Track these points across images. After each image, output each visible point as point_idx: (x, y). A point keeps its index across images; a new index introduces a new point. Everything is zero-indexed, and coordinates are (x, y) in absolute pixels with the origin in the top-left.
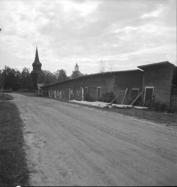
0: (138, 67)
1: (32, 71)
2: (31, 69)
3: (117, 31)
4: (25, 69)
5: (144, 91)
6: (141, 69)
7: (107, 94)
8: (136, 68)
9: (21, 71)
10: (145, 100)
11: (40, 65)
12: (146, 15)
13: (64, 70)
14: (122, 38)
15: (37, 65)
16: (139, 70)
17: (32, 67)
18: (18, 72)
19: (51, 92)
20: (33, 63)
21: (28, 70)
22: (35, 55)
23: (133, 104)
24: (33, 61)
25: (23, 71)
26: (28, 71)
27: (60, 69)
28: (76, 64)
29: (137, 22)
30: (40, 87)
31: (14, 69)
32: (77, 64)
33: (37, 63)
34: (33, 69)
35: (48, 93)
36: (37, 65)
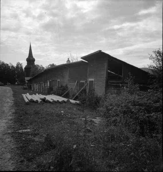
0: (83, 58)
1: (26, 66)
2: (24, 64)
3: (116, 27)
4: (18, 64)
5: (88, 84)
6: (83, 59)
7: (62, 86)
8: (80, 60)
9: (15, 65)
10: (65, 94)
11: (34, 60)
12: (144, 12)
13: (55, 65)
14: (120, 34)
15: (31, 60)
16: (83, 61)
17: (26, 62)
18: (13, 67)
19: (33, 85)
20: (27, 59)
21: (21, 65)
22: (29, 51)
23: (64, 96)
24: (27, 57)
25: (17, 66)
26: (22, 65)
27: (51, 64)
28: (68, 58)
29: (135, 19)
30: (27, 81)
31: (8, 63)
32: (68, 59)
33: (31, 58)
34: (27, 63)
35: (31, 86)
36: (31, 60)
